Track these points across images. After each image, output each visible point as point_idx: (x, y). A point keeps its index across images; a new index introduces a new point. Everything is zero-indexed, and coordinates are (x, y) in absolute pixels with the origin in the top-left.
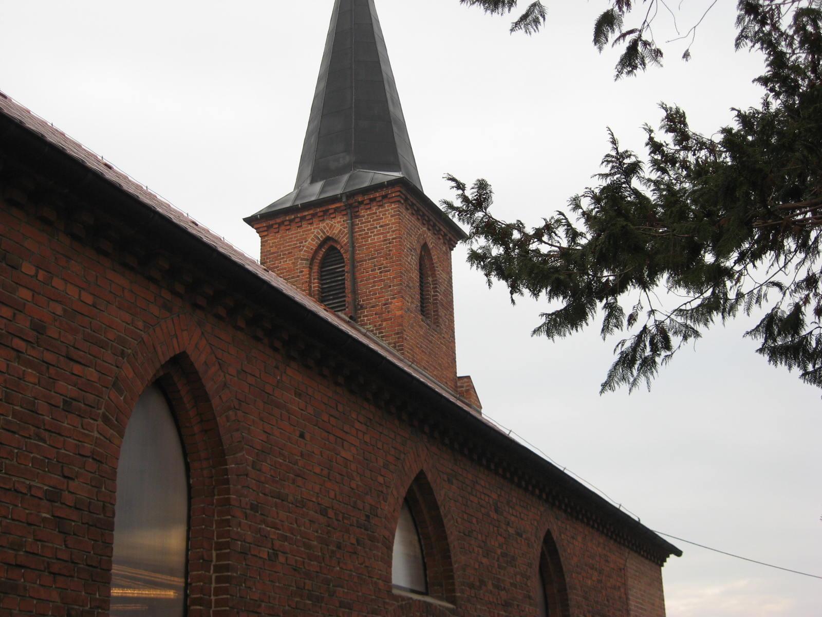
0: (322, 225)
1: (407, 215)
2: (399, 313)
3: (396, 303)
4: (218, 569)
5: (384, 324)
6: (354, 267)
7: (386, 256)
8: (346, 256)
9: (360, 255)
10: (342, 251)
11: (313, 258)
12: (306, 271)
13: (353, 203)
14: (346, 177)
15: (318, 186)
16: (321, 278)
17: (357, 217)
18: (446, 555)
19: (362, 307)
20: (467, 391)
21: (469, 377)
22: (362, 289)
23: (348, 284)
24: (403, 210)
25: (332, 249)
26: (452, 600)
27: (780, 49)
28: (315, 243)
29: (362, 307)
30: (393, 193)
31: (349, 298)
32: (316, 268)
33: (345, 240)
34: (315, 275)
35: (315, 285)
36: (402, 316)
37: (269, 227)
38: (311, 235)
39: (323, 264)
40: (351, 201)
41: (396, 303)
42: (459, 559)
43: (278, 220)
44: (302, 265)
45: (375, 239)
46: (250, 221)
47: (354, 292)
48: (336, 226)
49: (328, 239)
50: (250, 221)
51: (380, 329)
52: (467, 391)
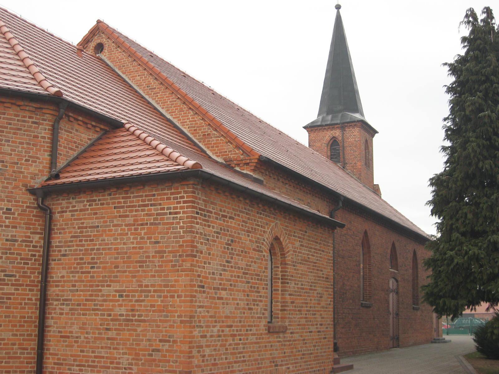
0: (331, 132)
1: (362, 131)
2: (360, 167)
3: (359, 164)
4: (369, 269)
5: (355, 170)
6: (344, 149)
7: (355, 146)
8: (341, 144)
9: (346, 145)
10: (339, 142)
11: (328, 143)
12: (326, 148)
13: (343, 126)
14: (340, 115)
15: (330, 117)
16: (331, 150)
17: (345, 131)
18: (396, 259)
19: (346, 163)
20: (378, 190)
21: (378, 185)
22: (346, 157)
23: (341, 154)
24: (361, 130)
25: (335, 140)
26: (397, 270)
27: (477, 229)
28: (329, 138)
29: (346, 163)
30: (359, 124)
31: (342, 159)
32: (329, 147)
33: (340, 139)
34: (329, 150)
35: (329, 153)
36: (361, 168)
37: (312, 130)
38: (328, 135)
39: (331, 146)
40: (343, 125)
41: (359, 164)
42: (399, 260)
43: (316, 128)
44: (324, 145)
45: (351, 140)
46: (305, 128)
47: (344, 158)
48: (337, 133)
49: (334, 137)
50: (305, 128)
51: (353, 172)
52: (378, 190)
